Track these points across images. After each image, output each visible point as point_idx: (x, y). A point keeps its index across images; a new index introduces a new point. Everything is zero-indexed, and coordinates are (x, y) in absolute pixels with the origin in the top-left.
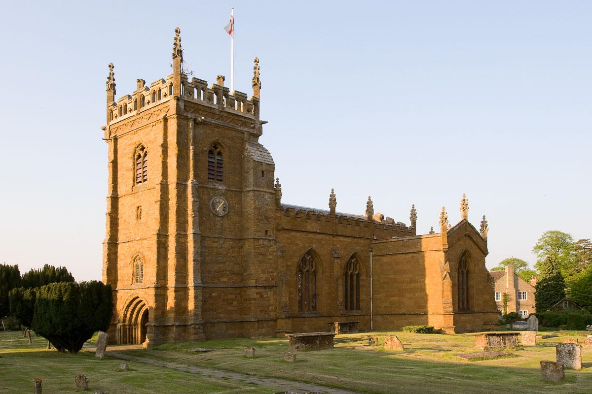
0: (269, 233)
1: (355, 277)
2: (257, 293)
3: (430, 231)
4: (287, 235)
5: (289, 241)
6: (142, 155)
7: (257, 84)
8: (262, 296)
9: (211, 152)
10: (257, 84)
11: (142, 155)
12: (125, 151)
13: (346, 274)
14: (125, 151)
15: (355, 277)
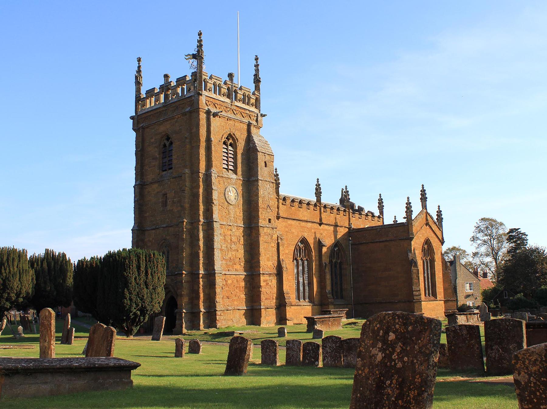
0: (272, 221)
1: (338, 266)
2: (265, 281)
3: (437, 210)
4: (284, 224)
5: (287, 229)
6: (167, 144)
7: (257, 81)
8: (267, 284)
9: (225, 143)
10: (257, 81)
11: (167, 144)
12: (153, 140)
13: (331, 261)
14: (153, 140)
15: (338, 266)
